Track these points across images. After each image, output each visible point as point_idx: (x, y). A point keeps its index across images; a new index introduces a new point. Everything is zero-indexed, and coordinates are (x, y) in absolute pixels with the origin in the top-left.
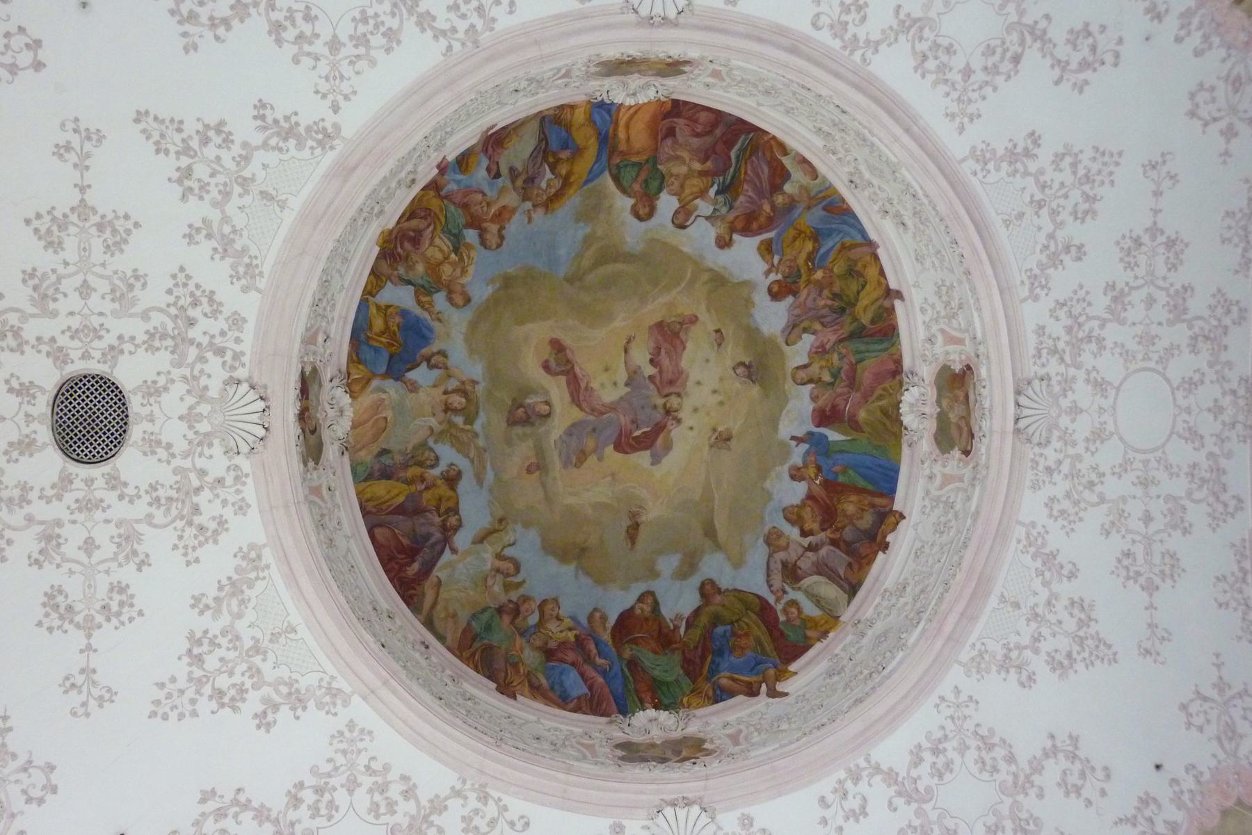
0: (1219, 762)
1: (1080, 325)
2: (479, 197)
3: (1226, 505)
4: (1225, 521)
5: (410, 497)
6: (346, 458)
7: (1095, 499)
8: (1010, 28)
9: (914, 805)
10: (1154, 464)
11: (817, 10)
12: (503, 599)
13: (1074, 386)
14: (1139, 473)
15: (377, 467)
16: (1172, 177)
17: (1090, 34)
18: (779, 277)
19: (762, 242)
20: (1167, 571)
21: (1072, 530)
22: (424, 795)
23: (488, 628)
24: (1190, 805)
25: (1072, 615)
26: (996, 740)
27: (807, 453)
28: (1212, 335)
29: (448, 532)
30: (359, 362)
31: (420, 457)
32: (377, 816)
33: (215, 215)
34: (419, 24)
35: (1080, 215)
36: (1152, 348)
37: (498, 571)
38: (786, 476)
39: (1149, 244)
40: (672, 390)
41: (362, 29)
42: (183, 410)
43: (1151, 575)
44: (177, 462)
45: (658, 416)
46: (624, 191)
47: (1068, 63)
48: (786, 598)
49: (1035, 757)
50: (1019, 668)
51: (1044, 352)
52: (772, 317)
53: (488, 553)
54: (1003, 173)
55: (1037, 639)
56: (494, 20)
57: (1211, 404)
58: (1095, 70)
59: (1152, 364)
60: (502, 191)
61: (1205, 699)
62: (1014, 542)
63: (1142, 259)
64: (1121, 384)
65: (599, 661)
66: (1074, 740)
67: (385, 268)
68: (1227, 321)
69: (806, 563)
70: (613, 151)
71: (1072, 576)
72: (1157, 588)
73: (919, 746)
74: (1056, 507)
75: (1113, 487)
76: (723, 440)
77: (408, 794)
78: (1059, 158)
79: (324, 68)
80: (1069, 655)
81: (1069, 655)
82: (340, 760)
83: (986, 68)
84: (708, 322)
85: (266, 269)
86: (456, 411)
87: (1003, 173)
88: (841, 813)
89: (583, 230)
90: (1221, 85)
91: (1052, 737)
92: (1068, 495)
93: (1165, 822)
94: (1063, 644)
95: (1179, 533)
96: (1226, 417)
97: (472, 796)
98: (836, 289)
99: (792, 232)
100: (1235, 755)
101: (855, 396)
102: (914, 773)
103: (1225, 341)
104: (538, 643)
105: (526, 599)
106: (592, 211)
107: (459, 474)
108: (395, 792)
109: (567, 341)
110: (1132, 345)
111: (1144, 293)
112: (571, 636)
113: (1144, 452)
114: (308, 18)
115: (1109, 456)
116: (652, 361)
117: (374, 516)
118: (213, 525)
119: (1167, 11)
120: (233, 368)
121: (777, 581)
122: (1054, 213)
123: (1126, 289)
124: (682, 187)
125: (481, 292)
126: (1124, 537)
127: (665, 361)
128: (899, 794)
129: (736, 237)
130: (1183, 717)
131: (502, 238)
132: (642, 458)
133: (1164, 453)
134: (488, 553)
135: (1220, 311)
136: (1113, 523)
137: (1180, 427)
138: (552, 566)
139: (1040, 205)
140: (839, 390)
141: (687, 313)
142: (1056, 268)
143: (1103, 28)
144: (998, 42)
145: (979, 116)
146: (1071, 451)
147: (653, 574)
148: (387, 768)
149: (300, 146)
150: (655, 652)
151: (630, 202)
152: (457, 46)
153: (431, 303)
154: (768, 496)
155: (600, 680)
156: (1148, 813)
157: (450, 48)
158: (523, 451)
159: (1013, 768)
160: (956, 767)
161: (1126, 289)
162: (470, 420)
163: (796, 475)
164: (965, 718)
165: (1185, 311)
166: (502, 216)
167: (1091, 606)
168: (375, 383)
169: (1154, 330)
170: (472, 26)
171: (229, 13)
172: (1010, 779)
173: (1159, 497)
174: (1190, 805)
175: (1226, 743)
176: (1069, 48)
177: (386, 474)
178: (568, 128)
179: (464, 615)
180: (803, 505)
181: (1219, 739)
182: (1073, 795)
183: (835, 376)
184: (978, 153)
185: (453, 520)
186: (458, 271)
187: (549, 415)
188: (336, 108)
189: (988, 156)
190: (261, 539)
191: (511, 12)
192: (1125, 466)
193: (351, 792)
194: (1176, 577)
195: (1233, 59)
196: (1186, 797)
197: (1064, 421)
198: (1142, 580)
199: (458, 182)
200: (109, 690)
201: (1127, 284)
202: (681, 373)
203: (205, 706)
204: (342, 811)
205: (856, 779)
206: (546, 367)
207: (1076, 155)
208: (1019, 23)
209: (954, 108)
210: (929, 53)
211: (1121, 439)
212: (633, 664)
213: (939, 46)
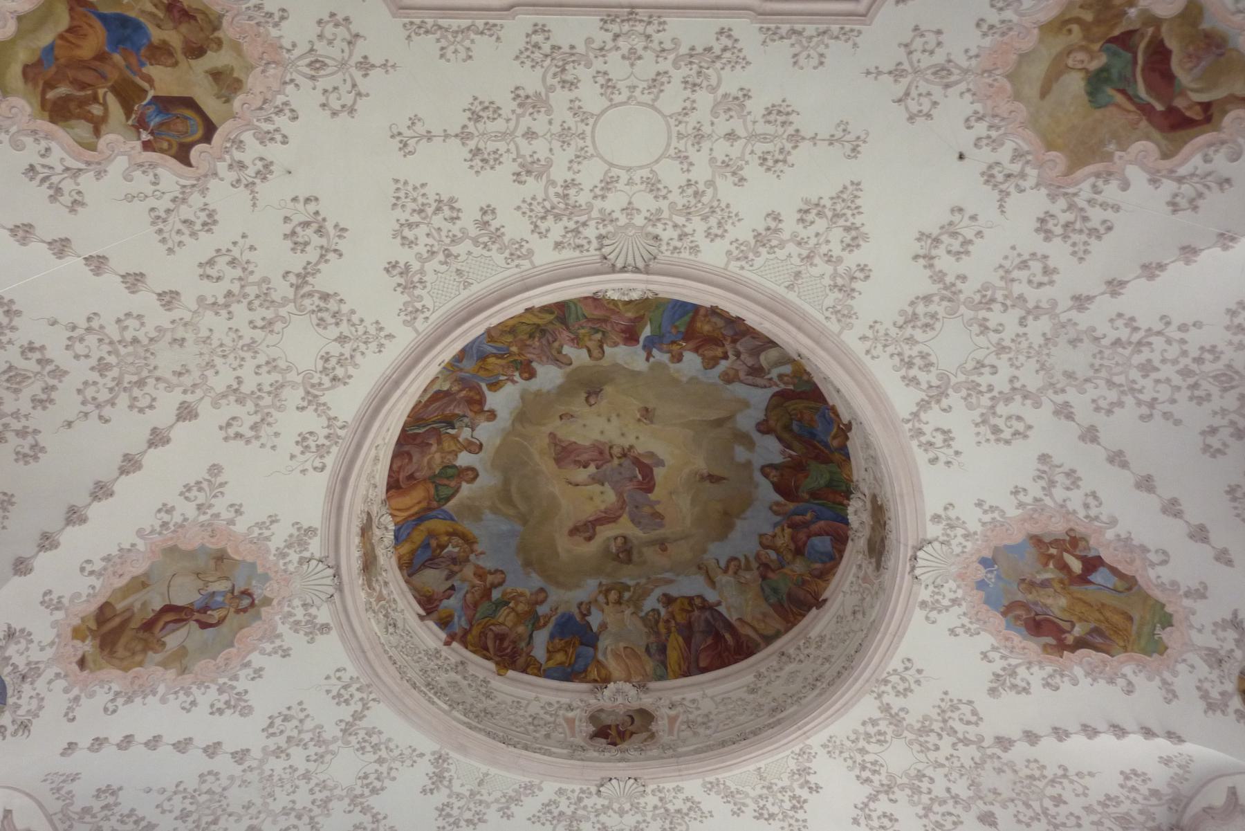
0: (969, 90)
1: (553, 208)
2: (469, 596)
3: (725, 49)
4: (740, 51)
5: (680, 632)
6: (653, 685)
7: (710, 192)
8: (301, 309)
9: (950, 391)
10: (681, 128)
12: (756, 573)
13: (608, 211)
14: (690, 143)
15: (657, 657)
16: (413, 124)
17: (294, 233)
18: (517, 374)
19: (490, 390)
20: (783, 118)
21: (737, 215)
22: (877, 714)
23: (775, 591)
24: (1002, 131)
25: (812, 223)
26: (910, 310)
27: (660, 350)
28: (560, 63)
29: (706, 606)
30: (585, 671)
31: (651, 622)
32: (886, 742)
33: (495, 806)
34: (360, 719)
35: (455, 215)
36: (573, 131)
37: (736, 573)
38: (678, 365)
39: (476, 139)
40: (607, 452)
41: (368, 748)
42: (616, 816)
43: (785, 136)
44: (648, 819)
45: (627, 462)
46: (457, 490)
47: (322, 247)
48: (776, 379)
49: (931, 277)
50: (853, 278)
51: (578, 242)
52: (549, 376)
53: (723, 579)
54: (423, 293)
55: (829, 259)
56: (351, 678)
57: (627, 62)
58: (324, 220)
59: (588, 129)
60: (464, 580)
61: (907, 94)
62: (744, 273)
63: (491, 146)
64: (606, 161)
65: (809, 516)
66: (922, 236)
67: (521, 661)
68: (546, 48)
69: (750, 361)
70: (429, 509)
71: (777, 218)
72: (797, 131)
73: (904, 378)
74: (715, 230)
75: (701, 172)
76: (647, 414)
77: (874, 723)
78: (408, 243)
79: (397, 764)
80: (847, 229)
81: (847, 229)
82: (846, 755)
83: (337, 324)
84: (554, 425)
85: (527, 780)
86: (620, 597)
87: (423, 293)
88: (945, 450)
89: (488, 515)
90: (322, 83)
91: (916, 257)
92: (705, 218)
93: (1012, 161)
94: (837, 234)
95: (748, 103)
96: (639, 44)
97: (883, 688)
98: (525, 337)
99: (482, 373)
100: (966, 71)
101: (614, 318)
102: (924, 386)
103: (566, 49)
104: (790, 557)
105: (758, 557)
106: (473, 511)
107: (665, 595)
108: (871, 730)
109: (570, 524)
110: (571, 152)
111: (523, 143)
112: (788, 531)
113: (670, 138)
114: (366, 777)
115: (671, 175)
116: (585, 467)
117: (692, 667)
118: (689, 804)
119: (262, 159)
120: (590, 793)
121: (759, 381)
122: (455, 240)
123: (519, 160)
124: (450, 452)
125: (536, 581)
126: (747, 163)
127: (585, 457)
128: (938, 402)
129: (486, 408)
130: (920, 121)
131: (496, 571)
132: (659, 473)
133: (671, 116)
134: (723, 579)
135: (537, 55)
136: (734, 174)
137: (647, 98)
138: (735, 535)
139: (448, 255)
140: (609, 328)
141: (547, 440)
142: (503, 234)
143: (287, 219)
144: (313, 316)
145: (377, 322)
146: (665, 215)
147: (748, 465)
148: (855, 732)
149: (448, 770)
150: (806, 477)
151: (465, 486)
152: (372, 696)
153: (545, 616)
154: (693, 380)
155: (822, 523)
156: (1000, 177)
157: (374, 700)
158: (650, 554)
159: (936, 299)
160: (926, 350)
161: (519, 160)
162: (627, 588)
163: (678, 358)
164: (887, 334)
165: (538, 95)
166: (481, 574)
167: (807, 202)
168: (600, 657)
169: (556, 128)
170: (358, 689)
171: (369, 815)
172: (945, 303)
173: (712, 124)
174: (1002, 131)
175: (953, 78)
176: (308, 249)
177: (663, 650)
178: (413, 553)
179: (765, 608)
180: (703, 356)
181: (947, 86)
182: (970, 248)
183: (597, 331)
184: (408, 318)
185: (697, 602)
186: (522, 599)
187: (625, 538)
188: (422, 755)
189: (410, 309)
190: (700, 781)
192: (682, 158)
193: (867, 752)
194: (789, 109)
195: (295, 76)
196: (994, 134)
197: (639, 220)
198: (788, 146)
199: (460, 618)
200: (838, 125)
201: (514, 160)
202: (594, 446)
203: (800, 815)
204: (878, 758)
205: (920, 433)
206: (590, 539)
207: (402, 225)
208: (295, 301)
209: (373, 346)
210: (331, 375)
211: (657, 161)
212: (814, 495)
213: (325, 369)
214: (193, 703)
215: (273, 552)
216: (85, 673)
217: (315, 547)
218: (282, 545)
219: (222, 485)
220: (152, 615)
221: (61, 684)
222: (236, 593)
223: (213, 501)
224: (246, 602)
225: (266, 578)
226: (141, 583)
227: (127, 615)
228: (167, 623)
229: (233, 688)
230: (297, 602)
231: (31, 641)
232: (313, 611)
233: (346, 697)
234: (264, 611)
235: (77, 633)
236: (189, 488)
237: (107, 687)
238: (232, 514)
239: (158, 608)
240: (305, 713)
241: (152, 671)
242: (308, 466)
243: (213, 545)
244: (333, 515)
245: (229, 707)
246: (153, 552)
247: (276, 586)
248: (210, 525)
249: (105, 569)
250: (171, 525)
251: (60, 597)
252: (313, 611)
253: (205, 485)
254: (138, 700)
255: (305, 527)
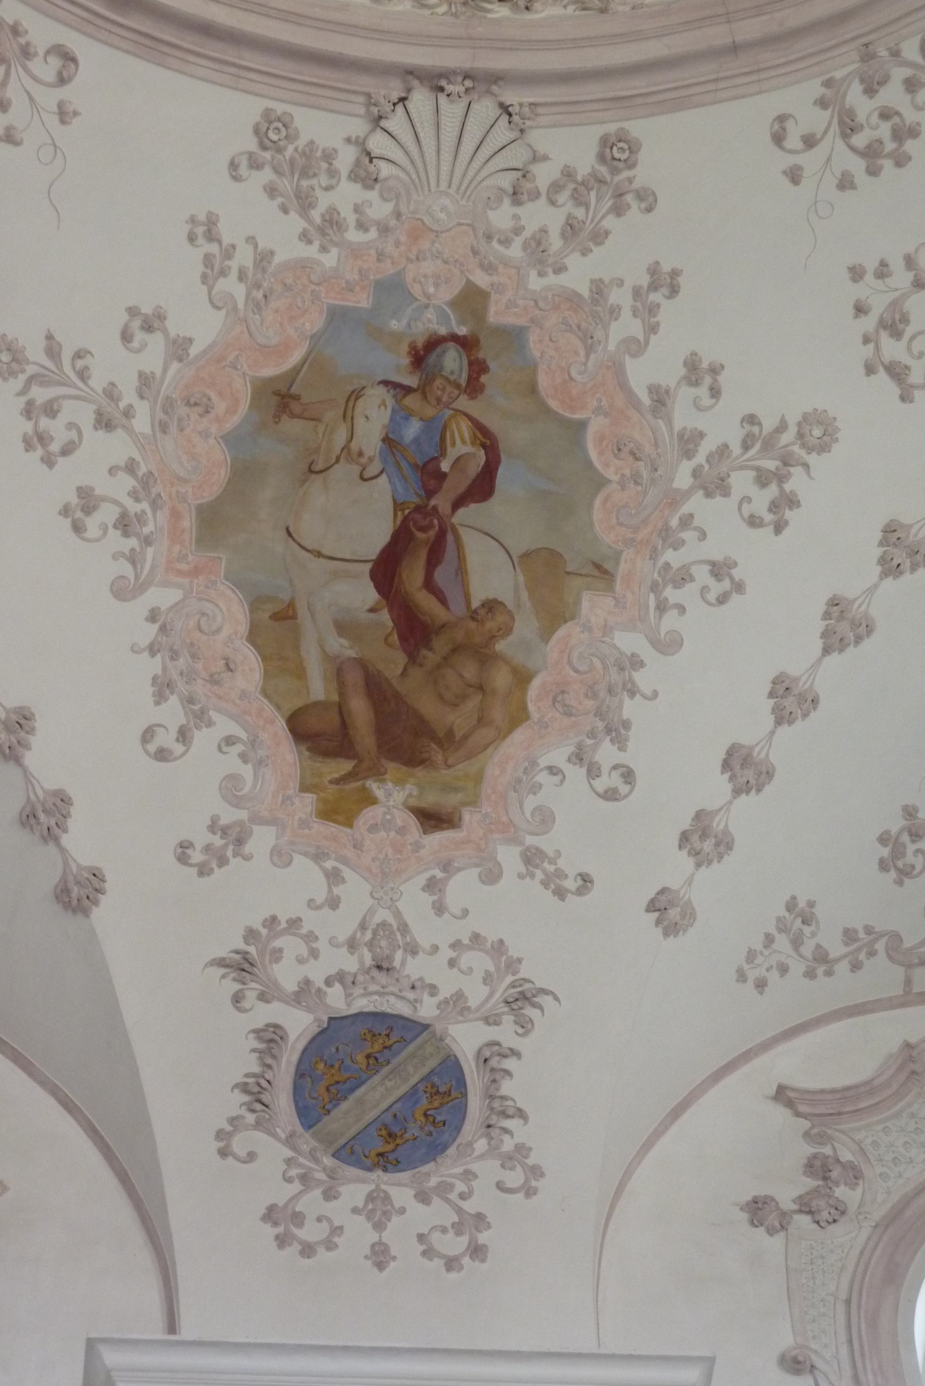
11: (64, 93)
170: (870, 91)
191: (782, 119)
214: (718, 570)
215: (312, 251)
216: (467, 816)
217: (326, 127)
218: (295, 222)
219: (53, 350)
220: (385, 617)
221: (463, 887)
222: (411, 381)
223: (98, 382)
224: (452, 361)
225: (392, 289)
226: (276, 624)
227: (354, 677)
228: (429, 585)
229: (724, 450)
230: (501, 217)
231: (295, 923)
232: (544, 175)
233: (885, 130)
234: (497, 314)
235: (339, 810)
236: (37, 440)
237: (543, 777)
238: (156, 344)
239: (372, 595)
240: (897, 265)
241: (556, 659)
242: (49, 98)
243: (235, 408)
244: (230, 54)
245: (781, 479)
246: (195, 572)
247: (428, 267)
248: (169, 405)
249: (190, 700)
250: (134, 507)
251: (213, 826)
252: (544, 175)
253: (40, 394)
254: (630, 708)
255: (251, 144)
